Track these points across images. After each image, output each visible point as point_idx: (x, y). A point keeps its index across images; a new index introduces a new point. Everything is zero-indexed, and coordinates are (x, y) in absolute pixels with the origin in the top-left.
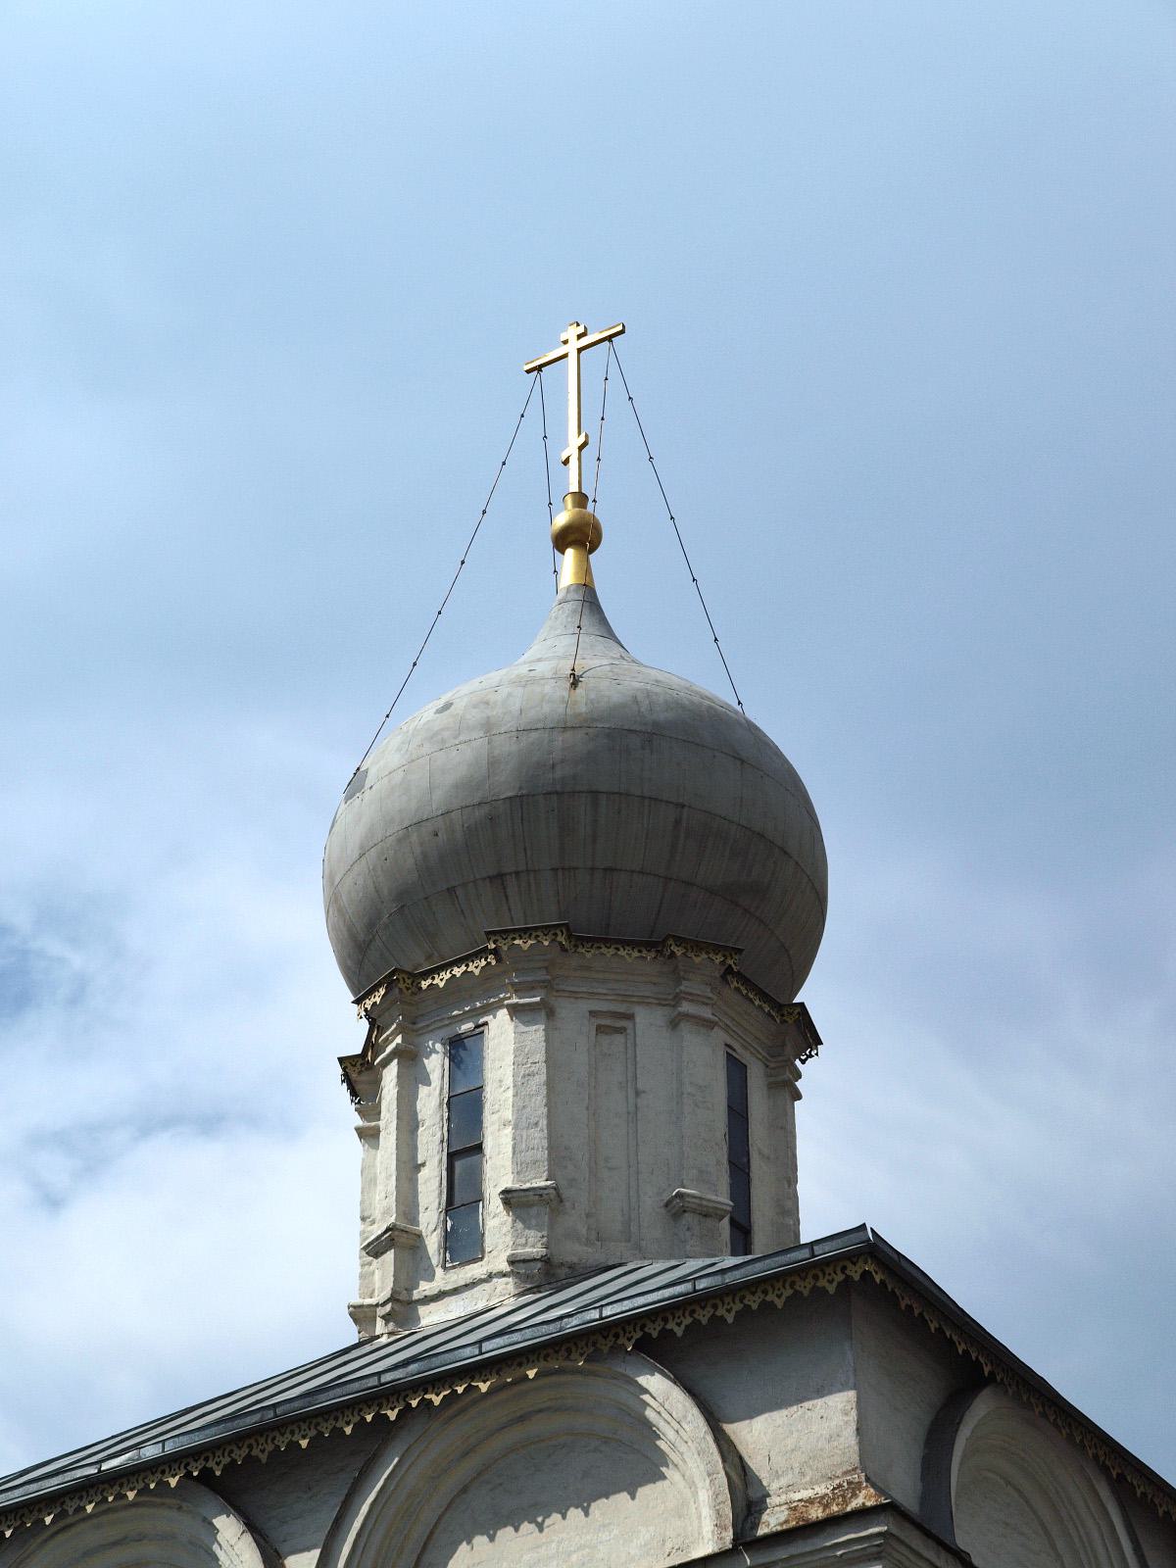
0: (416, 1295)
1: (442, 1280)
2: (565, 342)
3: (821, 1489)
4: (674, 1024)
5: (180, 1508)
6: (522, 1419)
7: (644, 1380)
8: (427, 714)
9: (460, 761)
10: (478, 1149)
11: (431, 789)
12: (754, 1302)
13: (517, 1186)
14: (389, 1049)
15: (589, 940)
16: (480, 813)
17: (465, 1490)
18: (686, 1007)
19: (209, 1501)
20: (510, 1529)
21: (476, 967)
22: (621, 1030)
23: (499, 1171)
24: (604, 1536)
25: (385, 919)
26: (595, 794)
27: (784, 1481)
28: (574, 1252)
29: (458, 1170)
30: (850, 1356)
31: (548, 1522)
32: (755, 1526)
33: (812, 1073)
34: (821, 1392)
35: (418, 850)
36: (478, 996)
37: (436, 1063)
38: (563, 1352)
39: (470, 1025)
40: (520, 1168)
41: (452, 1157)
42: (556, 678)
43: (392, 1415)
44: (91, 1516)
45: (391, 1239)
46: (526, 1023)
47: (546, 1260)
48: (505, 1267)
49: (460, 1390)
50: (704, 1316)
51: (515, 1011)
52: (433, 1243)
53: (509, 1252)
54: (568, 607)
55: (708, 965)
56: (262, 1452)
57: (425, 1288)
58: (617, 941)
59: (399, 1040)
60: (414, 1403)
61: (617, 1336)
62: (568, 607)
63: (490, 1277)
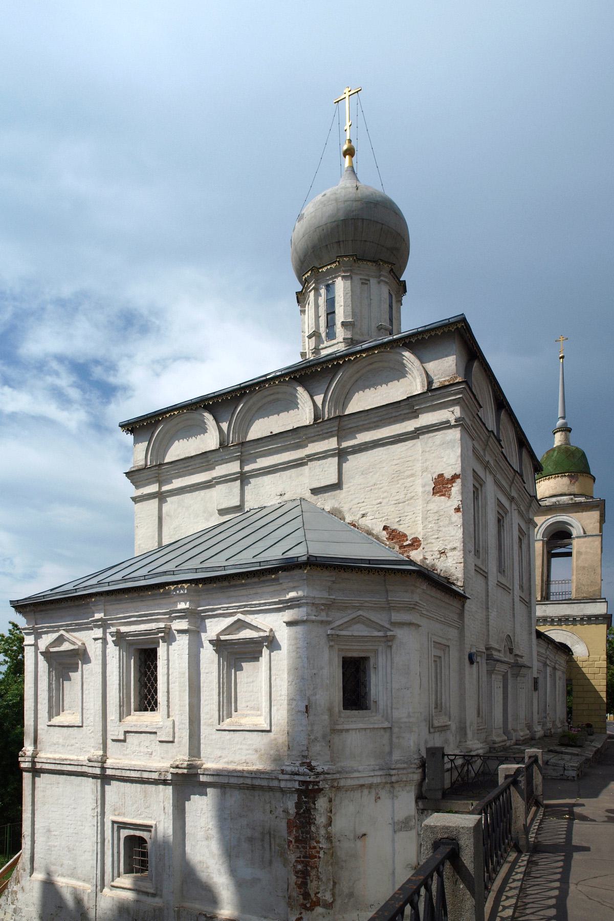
0: (320, 348)
1: (326, 344)
2: (345, 93)
3: (447, 378)
4: (379, 283)
5: (288, 386)
6: (371, 364)
7: (403, 353)
8: (319, 197)
9: (330, 209)
10: (334, 312)
11: (322, 217)
12: (433, 334)
13: (345, 321)
14: (311, 288)
15: (360, 259)
16: (334, 224)
17: (356, 381)
18: (382, 278)
19: (295, 384)
20: (368, 389)
21: (333, 266)
22: (367, 284)
23: (340, 316)
24: (391, 391)
25: (309, 253)
26: (363, 219)
27: (437, 377)
28: (357, 337)
29: (329, 318)
30: (454, 347)
31: (378, 387)
32: (432, 387)
33: (405, 299)
34: (447, 356)
35: (318, 234)
36: (334, 273)
37: (323, 291)
38: (384, 347)
39: (331, 281)
40: (345, 316)
41: (328, 314)
42: (352, 187)
43: (341, 362)
44: (267, 388)
45: (314, 334)
46: (346, 280)
47: (352, 339)
48: (342, 340)
49: (358, 356)
50: (446, 330)
51: (343, 277)
52: (323, 335)
53: (343, 337)
54: (348, 172)
55: (387, 267)
56: (308, 372)
57: (322, 346)
58: (367, 260)
59: (314, 285)
60: (347, 360)
61: (397, 343)
62: (348, 172)
63: (338, 343)
